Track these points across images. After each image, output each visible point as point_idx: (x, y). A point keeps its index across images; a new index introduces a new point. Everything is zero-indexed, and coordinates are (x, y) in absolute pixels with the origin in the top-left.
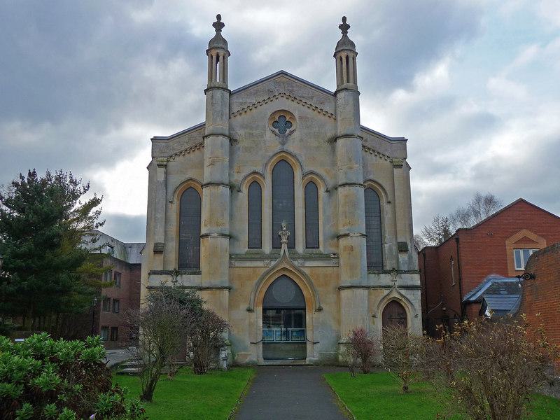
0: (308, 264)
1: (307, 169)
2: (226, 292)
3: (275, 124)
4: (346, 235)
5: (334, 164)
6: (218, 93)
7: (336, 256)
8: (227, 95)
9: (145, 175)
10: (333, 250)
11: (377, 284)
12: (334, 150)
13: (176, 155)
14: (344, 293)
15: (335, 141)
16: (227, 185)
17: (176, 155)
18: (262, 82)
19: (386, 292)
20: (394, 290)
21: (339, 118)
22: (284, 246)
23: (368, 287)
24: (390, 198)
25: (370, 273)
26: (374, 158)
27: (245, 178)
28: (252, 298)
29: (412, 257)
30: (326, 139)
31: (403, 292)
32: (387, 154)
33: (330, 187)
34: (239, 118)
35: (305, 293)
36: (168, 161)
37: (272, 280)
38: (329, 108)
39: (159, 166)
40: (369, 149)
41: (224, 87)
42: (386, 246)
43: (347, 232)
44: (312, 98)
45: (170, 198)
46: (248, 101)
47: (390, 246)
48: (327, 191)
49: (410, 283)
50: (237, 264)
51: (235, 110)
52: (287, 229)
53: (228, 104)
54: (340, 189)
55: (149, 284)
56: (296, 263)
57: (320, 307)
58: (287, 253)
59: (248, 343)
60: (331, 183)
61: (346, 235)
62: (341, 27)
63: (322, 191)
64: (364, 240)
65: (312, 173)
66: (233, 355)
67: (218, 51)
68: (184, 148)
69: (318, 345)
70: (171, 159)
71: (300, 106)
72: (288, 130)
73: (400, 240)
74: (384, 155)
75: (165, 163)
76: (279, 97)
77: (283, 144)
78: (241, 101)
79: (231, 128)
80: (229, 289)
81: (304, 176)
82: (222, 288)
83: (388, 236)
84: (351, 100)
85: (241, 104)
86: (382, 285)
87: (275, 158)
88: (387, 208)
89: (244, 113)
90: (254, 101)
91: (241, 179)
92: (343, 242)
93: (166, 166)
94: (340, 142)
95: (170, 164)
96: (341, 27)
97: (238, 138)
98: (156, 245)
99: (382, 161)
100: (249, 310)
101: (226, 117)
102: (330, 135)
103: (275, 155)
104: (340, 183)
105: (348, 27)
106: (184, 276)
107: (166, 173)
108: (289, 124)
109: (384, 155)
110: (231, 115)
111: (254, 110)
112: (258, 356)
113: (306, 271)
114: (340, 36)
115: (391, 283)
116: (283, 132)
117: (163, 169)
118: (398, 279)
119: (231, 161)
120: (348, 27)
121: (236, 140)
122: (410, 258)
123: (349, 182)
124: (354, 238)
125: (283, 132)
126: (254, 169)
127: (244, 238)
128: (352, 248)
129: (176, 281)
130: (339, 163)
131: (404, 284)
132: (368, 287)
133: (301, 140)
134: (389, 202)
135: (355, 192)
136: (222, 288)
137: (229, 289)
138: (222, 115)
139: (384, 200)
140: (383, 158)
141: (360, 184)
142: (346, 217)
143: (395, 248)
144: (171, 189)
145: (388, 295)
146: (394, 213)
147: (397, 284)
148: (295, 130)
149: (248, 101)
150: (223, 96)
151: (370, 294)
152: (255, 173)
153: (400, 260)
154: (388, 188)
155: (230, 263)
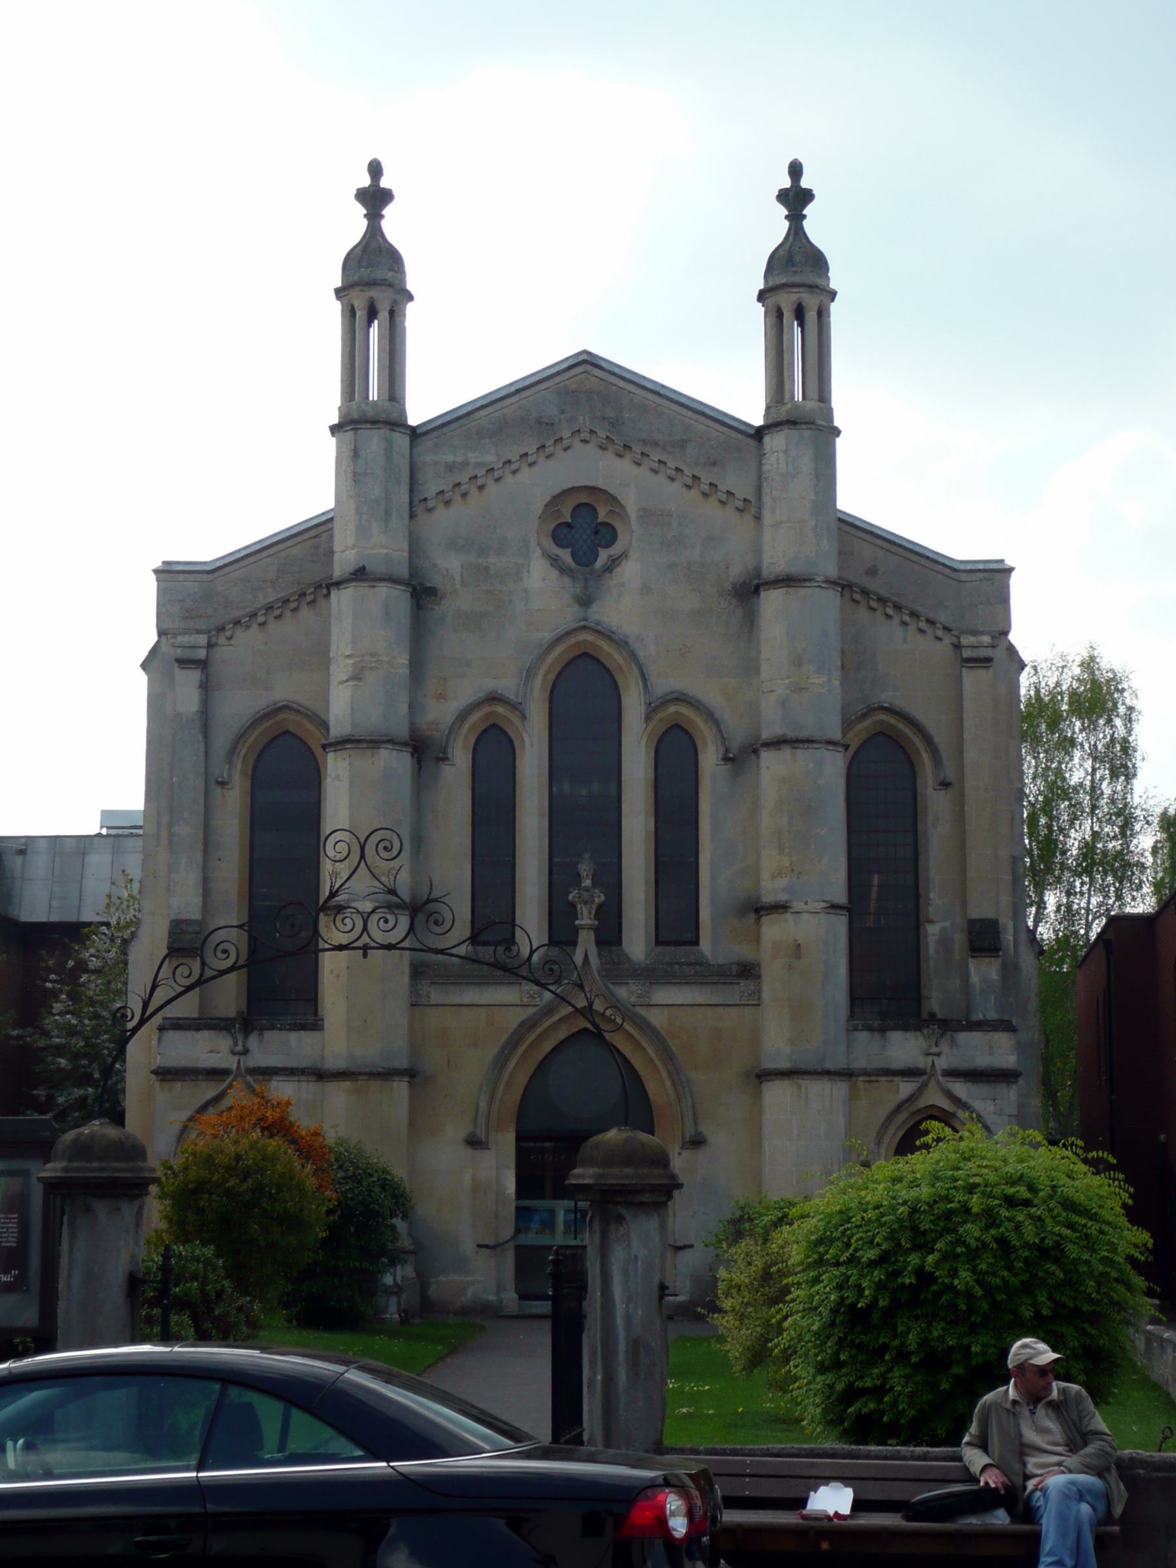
0: (665, 995)
1: (662, 685)
2: (401, 1088)
3: (561, 534)
4: (781, 908)
5: (750, 667)
6: (374, 440)
7: (748, 971)
8: (402, 441)
9: (139, 684)
10: (742, 951)
11: (876, 1064)
12: (750, 620)
13: (237, 623)
14: (777, 1094)
15: (756, 590)
16: (405, 744)
17: (237, 623)
18: (518, 391)
19: (906, 1088)
20: (932, 1084)
21: (768, 518)
22: (586, 943)
23: (847, 1074)
24: (950, 774)
25: (856, 1029)
26: (899, 631)
27: (463, 716)
28: (483, 1104)
29: (1016, 967)
30: (728, 586)
31: (960, 1088)
32: (942, 617)
33: (735, 745)
34: (441, 513)
35: (651, 1087)
36: (210, 646)
37: (548, 1046)
38: (736, 481)
39: (183, 662)
40: (882, 600)
41: (394, 416)
42: (932, 931)
43: (783, 897)
44: (683, 444)
45: (219, 769)
46: (473, 457)
47: (943, 929)
48: (726, 759)
49: (983, 1061)
50: (436, 996)
51: (431, 486)
52: (595, 884)
53: (405, 477)
54: (766, 756)
55: (159, 1061)
56: (622, 992)
57: (699, 1134)
58: (594, 960)
59: (468, 1246)
60: (738, 737)
61: (781, 908)
62: (784, 197)
63: (710, 760)
64: (841, 923)
65: (680, 698)
66: (424, 1286)
67: (374, 293)
68: (262, 601)
69: (687, 1255)
70: (222, 640)
71: (643, 471)
72: (603, 556)
73: (975, 913)
74: (931, 622)
75: (201, 654)
76: (577, 443)
77: (585, 601)
78: (449, 458)
79: (415, 548)
80: (411, 1074)
81: (652, 709)
82: (386, 1075)
83: (937, 899)
84: (806, 464)
85: (450, 468)
86: (896, 1065)
87: (559, 650)
88: (936, 803)
89: (458, 498)
90: (490, 458)
91: (449, 718)
92: (773, 930)
93: (203, 664)
94: (772, 601)
95: (224, 652)
96: (784, 197)
97: (436, 581)
98: (177, 928)
99: (925, 643)
100: (474, 1142)
101: (399, 522)
102: (737, 571)
103: (558, 640)
104: (765, 735)
105: (807, 196)
106: (268, 1035)
107: (205, 687)
108: (606, 534)
109: (931, 622)
110: (417, 505)
111: (492, 488)
112: (500, 1288)
113: (656, 1018)
114: (781, 228)
115: (922, 1062)
116: (585, 558)
117: (195, 676)
118: (944, 1047)
119: (417, 665)
120: (807, 196)
121: (432, 592)
122: (1010, 971)
123: (792, 735)
124: (805, 916)
125: (585, 558)
126: (490, 684)
127: (459, 907)
128: (797, 950)
129: (246, 1052)
130: (765, 669)
131: (964, 1065)
132: (847, 1074)
133: (645, 590)
134: (945, 785)
135: (180, 1321)
136: (386, 1075)
137: (411, 1074)
138: (388, 514)
139: (927, 774)
140: (929, 630)
141: (830, 742)
142: (781, 848)
143: (959, 939)
144: (221, 740)
145: (912, 1098)
146: (960, 818)
147: (942, 1063)
148: (624, 556)
149: (473, 457)
150: (389, 450)
151: (853, 1095)
152: (493, 698)
153: (974, 979)
154: (941, 738)
155: (414, 991)
